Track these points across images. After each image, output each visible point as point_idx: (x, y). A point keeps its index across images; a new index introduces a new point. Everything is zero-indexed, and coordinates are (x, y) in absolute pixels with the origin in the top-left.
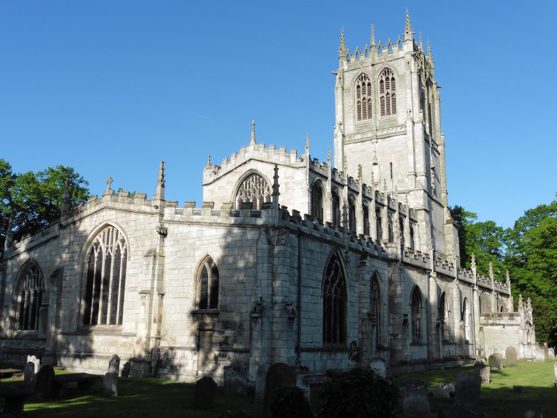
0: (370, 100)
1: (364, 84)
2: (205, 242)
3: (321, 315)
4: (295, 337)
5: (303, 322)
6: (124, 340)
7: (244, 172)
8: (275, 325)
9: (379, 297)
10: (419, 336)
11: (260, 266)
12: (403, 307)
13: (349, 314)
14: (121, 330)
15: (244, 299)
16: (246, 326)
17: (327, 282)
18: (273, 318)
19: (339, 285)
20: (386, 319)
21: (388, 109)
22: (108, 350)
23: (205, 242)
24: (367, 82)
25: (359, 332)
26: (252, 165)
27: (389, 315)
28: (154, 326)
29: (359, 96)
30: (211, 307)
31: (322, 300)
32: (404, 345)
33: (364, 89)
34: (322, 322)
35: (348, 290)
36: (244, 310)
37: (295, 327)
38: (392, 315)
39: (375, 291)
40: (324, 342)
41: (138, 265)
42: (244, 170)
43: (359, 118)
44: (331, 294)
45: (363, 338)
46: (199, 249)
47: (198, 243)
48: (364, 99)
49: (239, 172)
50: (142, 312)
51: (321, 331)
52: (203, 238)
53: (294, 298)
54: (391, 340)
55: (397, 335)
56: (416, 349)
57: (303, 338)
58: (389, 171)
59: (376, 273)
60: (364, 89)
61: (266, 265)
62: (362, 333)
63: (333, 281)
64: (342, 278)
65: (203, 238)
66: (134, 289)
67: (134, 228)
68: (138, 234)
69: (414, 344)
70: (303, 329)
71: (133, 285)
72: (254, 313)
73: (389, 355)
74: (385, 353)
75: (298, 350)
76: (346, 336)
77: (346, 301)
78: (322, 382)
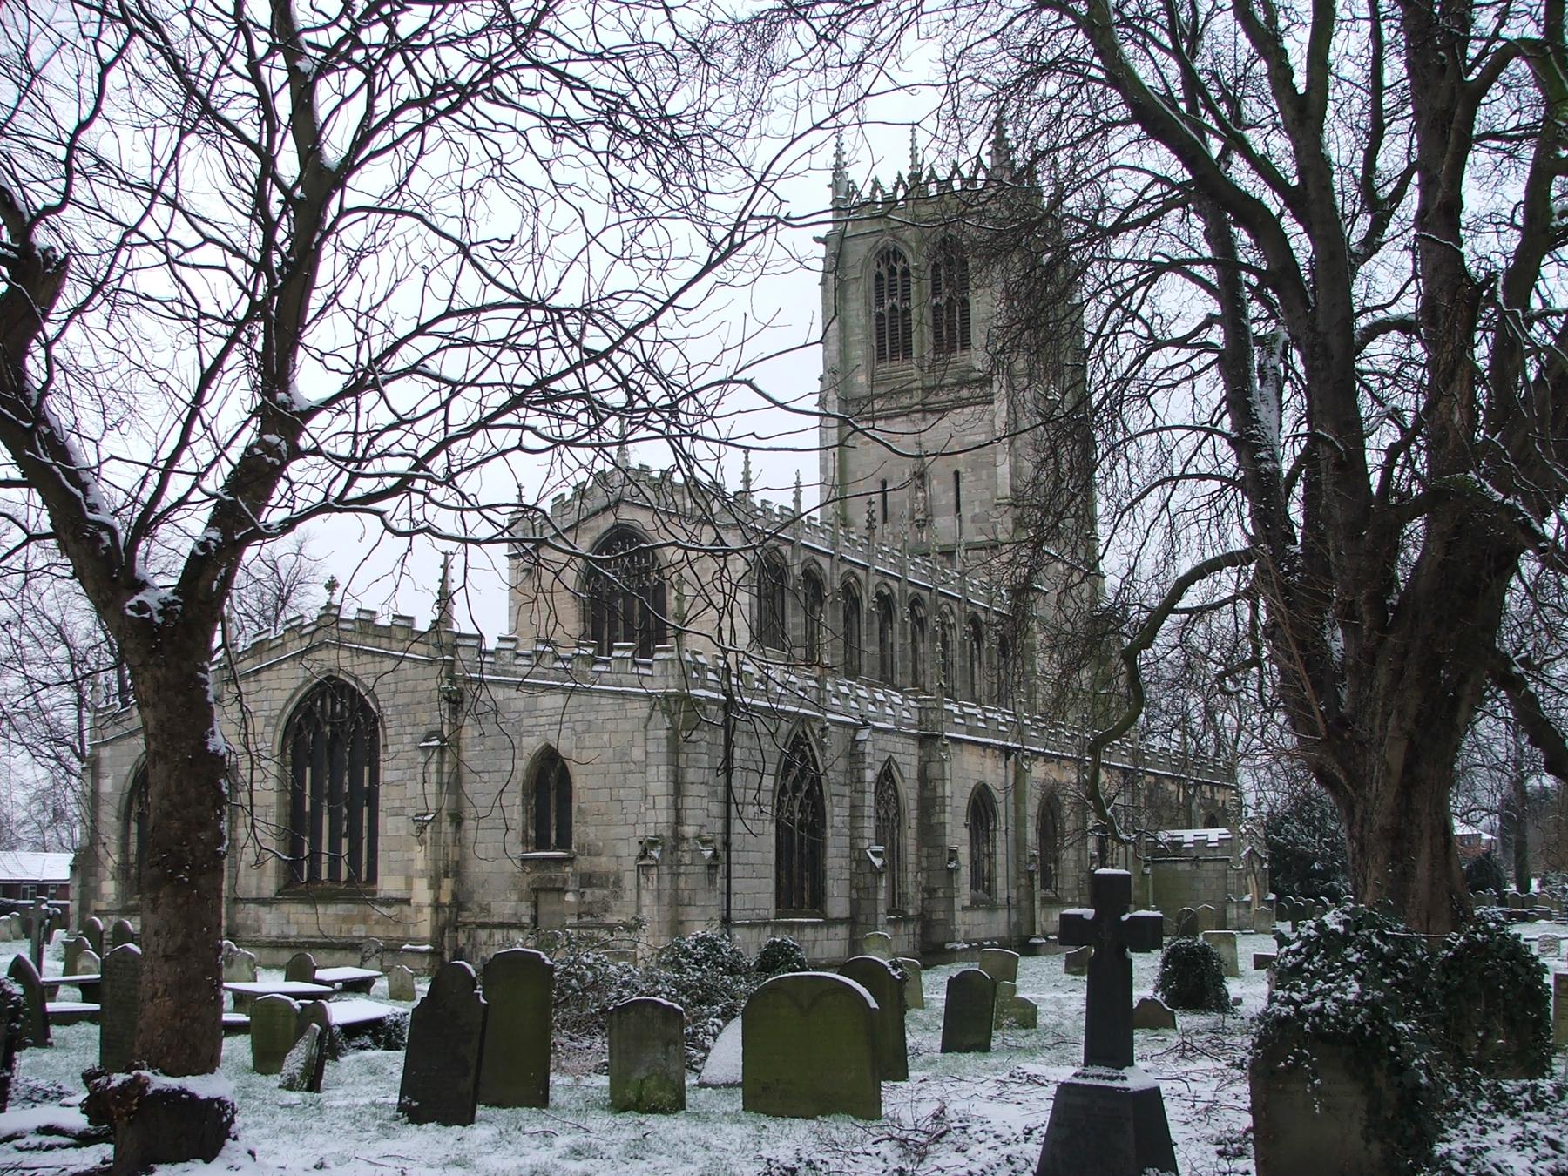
0: (907, 312)
1: (892, 271)
2: (543, 720)
3: (772, 856)
4: (722, 899)
5: (736, 871)
6: (385, 910)
7: (603, 530)
8: (682, 878)
9: (897, 813)
10: (990, 891)
11: (652, 770)
12: (948, 831)
13: (831, 851)
14: (375, 893)
15: (624, 831)
16: (629, 880)
17: (783, 791)
18: (679, 866)
19: (809, 793)
20: (912, 859)
21: (952, 338)
22: (349, 930)
23: (543, 720)
24: (899, 267)
25: (851, 888)
26: (626, 514)
27: (919, 850)
28: (448, 884)
29: (880, 303)
30: (558, 847)
31: (773, 828)
32: (950, 910)
33: (892, 283)
34: (773, 869)
35: (827, 802)
36: (623, 852)
37: (720, 881)
38: (925, 850)
39: (888, 803)
40: (778, 906)
41: (403, 763)
42: (606, 522)
43: (881, 357)
44: (792, 813)
45: (859, 898)
46: (531, 734)
47: (528, 721)
48: (893, 308)
49: (591, 530)
50: (420, 858)
51: (772, 888)
52: (538, 713)
53: (719, 825)
54: (923, 900)
55: (935, 890)
56: (979, 917)
57: (736, 902)
58: (952, 494)
59: (889, 769)
60: (892, 283)
61: (663, 768)
62: (858, 889)
63: (797, 787)
64: (817, 781)
65: (538, 713)
66: (398, 812)
67: (392, 687)
68: (401, 699)
69: (975, 905)
70: (736, 885)
71: (397, 804)
72: (642, 858)
73: (918, 931)
74: (911, 927)
75: (727, 922)
76: (824, 894)
77: (824, 826)
78: (137, 949)
